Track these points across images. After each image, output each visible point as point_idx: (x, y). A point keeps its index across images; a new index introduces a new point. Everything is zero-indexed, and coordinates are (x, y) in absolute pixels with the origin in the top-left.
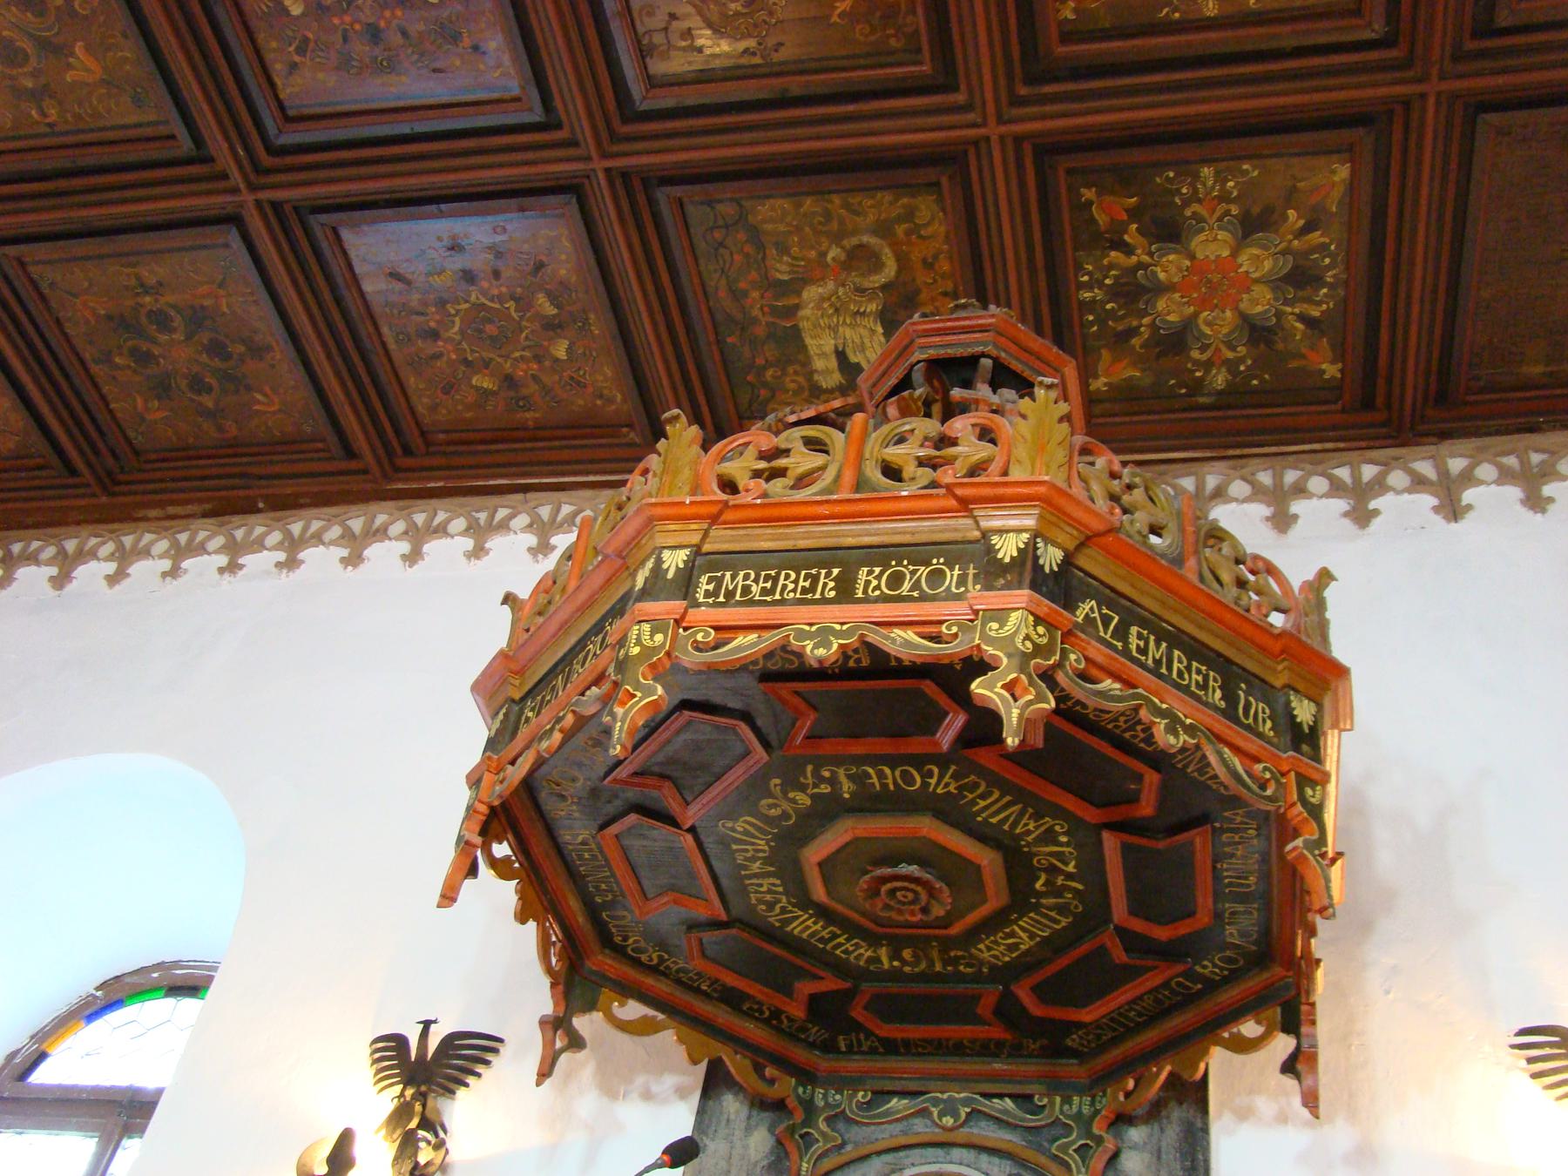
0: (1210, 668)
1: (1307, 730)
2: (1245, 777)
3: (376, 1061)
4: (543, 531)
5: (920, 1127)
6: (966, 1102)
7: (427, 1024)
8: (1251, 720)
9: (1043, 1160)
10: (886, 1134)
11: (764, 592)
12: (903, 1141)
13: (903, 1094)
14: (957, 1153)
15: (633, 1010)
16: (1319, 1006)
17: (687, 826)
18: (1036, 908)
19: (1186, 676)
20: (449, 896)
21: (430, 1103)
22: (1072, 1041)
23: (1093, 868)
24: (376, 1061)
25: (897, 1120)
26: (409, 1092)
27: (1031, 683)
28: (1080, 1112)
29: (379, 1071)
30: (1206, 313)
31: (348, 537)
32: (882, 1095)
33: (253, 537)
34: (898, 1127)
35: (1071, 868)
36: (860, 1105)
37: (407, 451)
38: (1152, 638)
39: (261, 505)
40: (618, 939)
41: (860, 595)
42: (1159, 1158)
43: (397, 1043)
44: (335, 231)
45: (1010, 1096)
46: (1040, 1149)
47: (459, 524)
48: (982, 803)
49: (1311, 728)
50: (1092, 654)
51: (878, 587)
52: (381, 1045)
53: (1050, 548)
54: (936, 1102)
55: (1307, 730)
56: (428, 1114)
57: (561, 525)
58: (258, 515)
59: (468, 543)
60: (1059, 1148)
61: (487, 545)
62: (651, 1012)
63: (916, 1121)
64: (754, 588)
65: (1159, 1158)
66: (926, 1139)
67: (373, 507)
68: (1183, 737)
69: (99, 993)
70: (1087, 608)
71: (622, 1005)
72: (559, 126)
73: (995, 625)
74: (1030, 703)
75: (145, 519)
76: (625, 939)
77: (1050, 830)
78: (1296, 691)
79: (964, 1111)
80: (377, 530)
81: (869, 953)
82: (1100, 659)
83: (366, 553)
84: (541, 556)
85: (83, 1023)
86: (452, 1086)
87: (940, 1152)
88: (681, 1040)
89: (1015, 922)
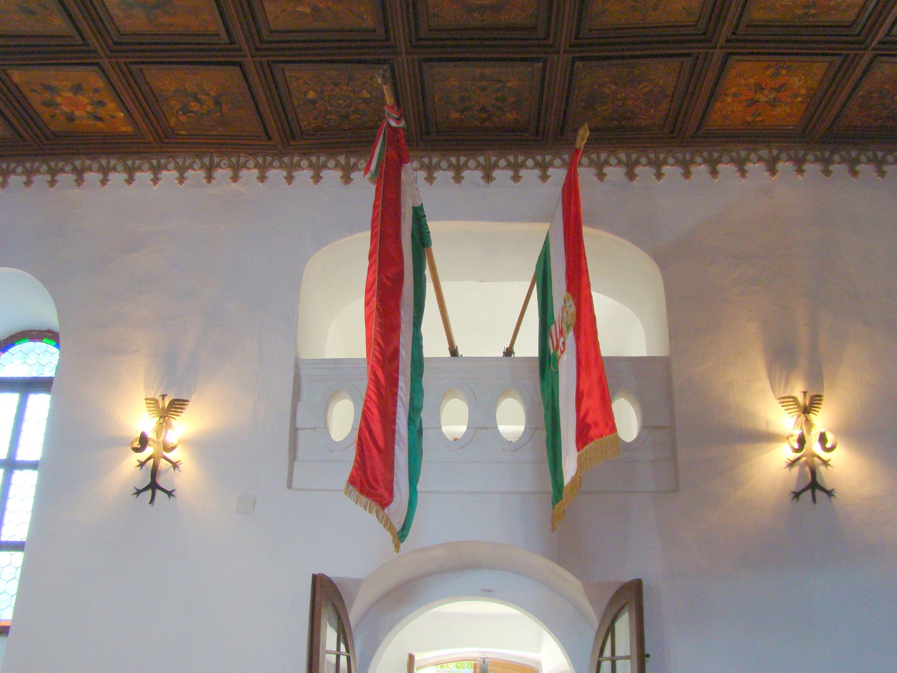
16: (391, 536)
30: (467, 103)
31: (75, 169)
37: (167, 137)
44: (283, 70)
47: (251, 163)
59: (24, 178)
61: (33, 179)
72: (235, 43)
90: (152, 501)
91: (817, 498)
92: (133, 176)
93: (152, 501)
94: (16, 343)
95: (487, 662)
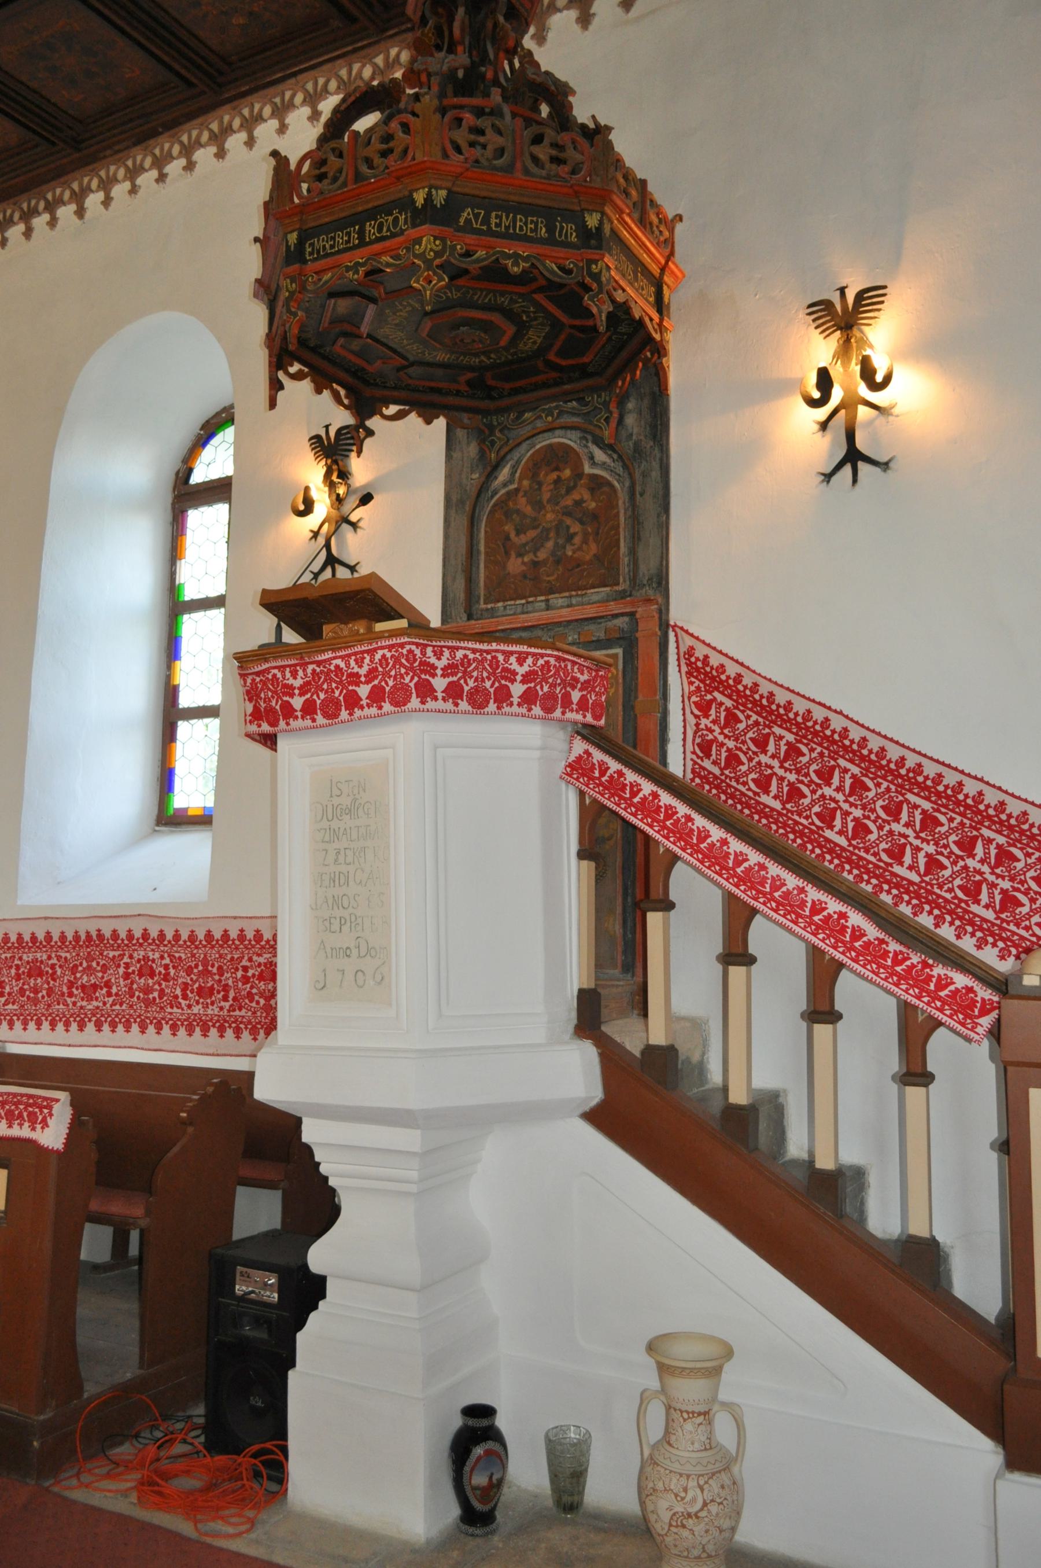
0: (538, 217)
1: (594, 230)
2: (560, 273)
3: (313, 449)
4: (313, 100)
5: (539, 424)
6: (557, 407)
7: (327, 427)
8: (563, 237)
9: (592, 427)
10: (526, 431)
11: (332, 247)
12: (535, 432)
13: (533, 409)
14: (557, 432)
15: (393, 409)
17: (365, 336)
18: (531, 327)
19: (525, 228)
20: (273, 404)
21: (340, 463)
22: (590, 369)
23: (540, 307)
24: (313, 449)
25: (529, 423)
26: (329, 461)
27: (435, 273)
28: (605, 400)
29: (315, 454)
32: (521, 414)
33: (165, 152)
34: (529, 427)
35: (532, 309)
36: (513, 421)
38: (504, 214)
39: (160, 130)
40: (372, 381)
41: (368, 240)
42: (641, 414)
43: (317, 438)
45: (575, 400)
46: (591, 423)
48: (476, 297)
49: (596, 228)
50: (468, 241)
51: (374, 234)
52: (313, 441)
53: (440, 192)
54: (543, 410)
55: (594, 230)
56: (342, 468)
57: (321, 95)
58: (161, 136)
60: (597, 421)
62: (402, 407)
63: (537, 421)
64: (327, 246)
65: (641, 414)
66: (542, 429)
67: (219, 112)
68: (522, 264)
69: (202, 432)
70: (465, 214)
71: (387, 408)
73: (417, 247)
74: (436, 284)
75: (105, 157)
76: (375, 380)
77: (511, 299)
78: (588, 210)
79: (556, 412)
80: (226, 128)
81: (477, 360)
82: (472, 242)
83: (86, 206)
84: (315, 122)
85: (201, 449)
86: (346, 453)
87: (550, 434)
88: (420, 416)
89: (527, 333)
90: (855, 481)
91: (860, 474)
92: (84, 203)
93: (855, 481)
94: (179, 634)
95: (683, 1063)
